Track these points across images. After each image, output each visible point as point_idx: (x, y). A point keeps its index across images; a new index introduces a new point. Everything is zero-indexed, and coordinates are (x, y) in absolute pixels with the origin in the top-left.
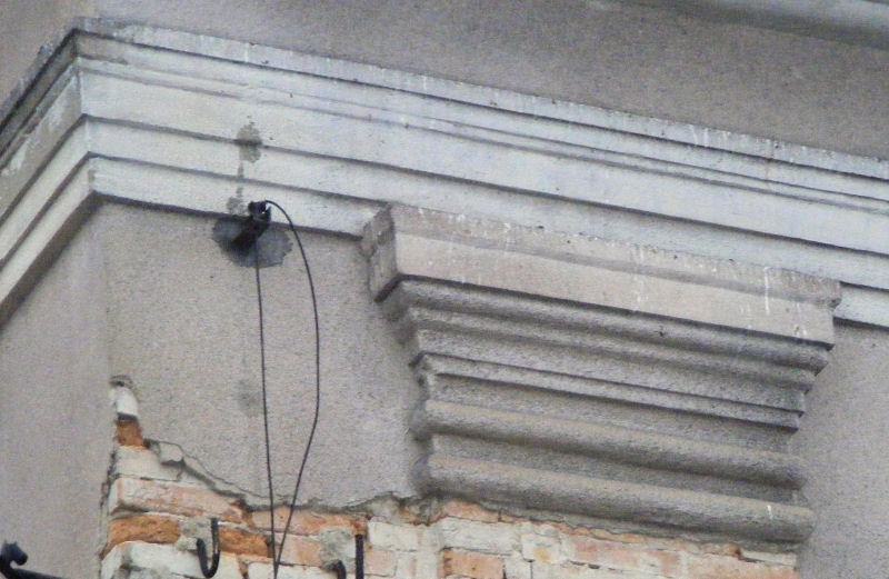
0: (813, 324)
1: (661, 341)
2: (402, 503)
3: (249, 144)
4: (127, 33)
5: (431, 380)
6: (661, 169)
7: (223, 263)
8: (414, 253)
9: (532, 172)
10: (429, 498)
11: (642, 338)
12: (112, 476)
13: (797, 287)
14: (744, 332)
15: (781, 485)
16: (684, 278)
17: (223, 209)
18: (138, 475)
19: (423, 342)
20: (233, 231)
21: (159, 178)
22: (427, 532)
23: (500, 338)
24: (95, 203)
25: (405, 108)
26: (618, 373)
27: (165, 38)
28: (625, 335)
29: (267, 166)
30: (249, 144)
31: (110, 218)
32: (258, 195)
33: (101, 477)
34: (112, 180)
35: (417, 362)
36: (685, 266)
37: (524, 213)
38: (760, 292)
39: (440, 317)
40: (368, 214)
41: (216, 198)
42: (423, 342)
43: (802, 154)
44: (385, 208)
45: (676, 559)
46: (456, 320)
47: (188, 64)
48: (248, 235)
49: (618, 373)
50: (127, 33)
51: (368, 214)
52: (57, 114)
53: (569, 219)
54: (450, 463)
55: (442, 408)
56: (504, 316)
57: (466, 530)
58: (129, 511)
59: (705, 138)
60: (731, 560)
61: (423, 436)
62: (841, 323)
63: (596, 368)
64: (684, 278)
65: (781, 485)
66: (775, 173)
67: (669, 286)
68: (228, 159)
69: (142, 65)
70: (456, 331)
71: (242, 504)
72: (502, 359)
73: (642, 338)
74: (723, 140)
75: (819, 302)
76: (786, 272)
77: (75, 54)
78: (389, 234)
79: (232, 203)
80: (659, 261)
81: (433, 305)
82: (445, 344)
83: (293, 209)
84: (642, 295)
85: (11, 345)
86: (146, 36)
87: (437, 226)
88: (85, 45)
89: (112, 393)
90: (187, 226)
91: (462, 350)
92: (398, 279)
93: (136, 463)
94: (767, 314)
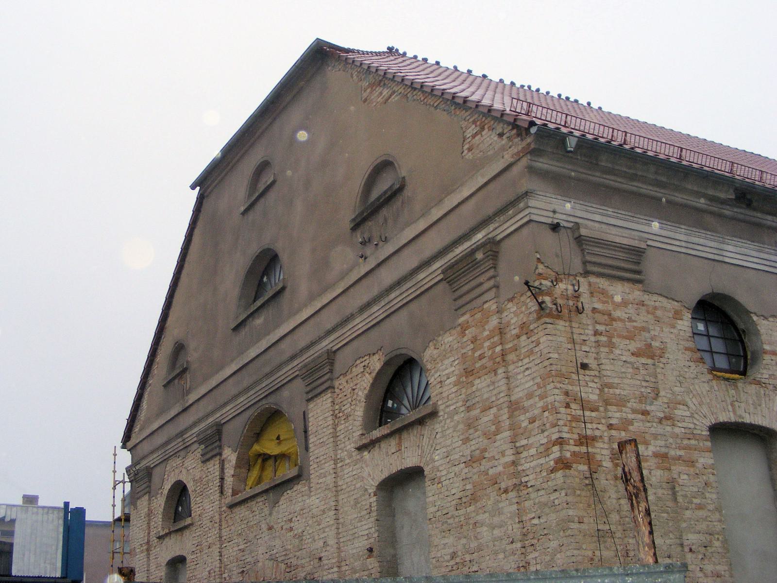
0: (643, 246)
1: (621, 248)
2: (581, 274)
3: (554, 212)
4: (535, 192)
5: (585, 253)
6: (617, 218)
7: (551, 233)
8: (583, 232)
9: (598, 218)
10: (586, 273)
11: (618, 247)
12: (537, 268)
13: (641, 240)
14: (633, 246)
15: (639, 272)
16: (623, 237)
17: (550, 223)
18: (541, 268)
19: (584, 246)
20: (552, 227)
21: (705, 253)
22: (585, 279)
23: (596, 246)
24: (530, 221)
25: (610, 211)
26: (614, 253)
27: (541, 193)
28: (615, 246)
29: (557, 216)
30: (554, 212)
31: (531, 225)
32: (558, 221)
33: (534, 268)
34: (534, 218)
35: (583, 250)
36: (624, 235)
37: (597, 225)
38: (635, 240)
39: (587, 243)
40: (572, 224)
41: (549, 221)
42: (584, 246)
43: (638, 216)
44: (577, 223)
45: (624, 285)
46: (590, 243)
47: (545, 198)
48: (555, 227)
49: (614, 253)
50: (535, 192)
51: (572, 224)
52: (522, 205)
53: (604, 226)
54: (590, 268)
55: (588, 258)
56: (597, 243)
57: (593, 279)
58: (540, 274)
59: (623, 213)
60: (632, 285)
61: (585, 263)
62: (648, 245)
63: (610, 252)
64: (623, 237)
65: (639, 272)
66: (635, 219)
67: (621, 238)
68: (551, 214)
69: (538, 198)
70: (588, 245)
71: (557, 273)
72: (597, 250)
73: (618, 247)
74: (627, 213)
75: (644, 242)
76: (639, 236)
77: (527, 195)
78: (579, 228)
79: (552, 222)
80: (620, 234)
81: (588, 241)
82: (588, 247)
83: (563, 224)
84: (618, 240)
85: (740, 384)
86: (538, 193)
87: (586, 227)
88: (529, 194)
89: (536, 254)
90: (544, 226)
91: (590, 248)
92: (581, 236)
93: (541, 266)
94: (635, 243)
